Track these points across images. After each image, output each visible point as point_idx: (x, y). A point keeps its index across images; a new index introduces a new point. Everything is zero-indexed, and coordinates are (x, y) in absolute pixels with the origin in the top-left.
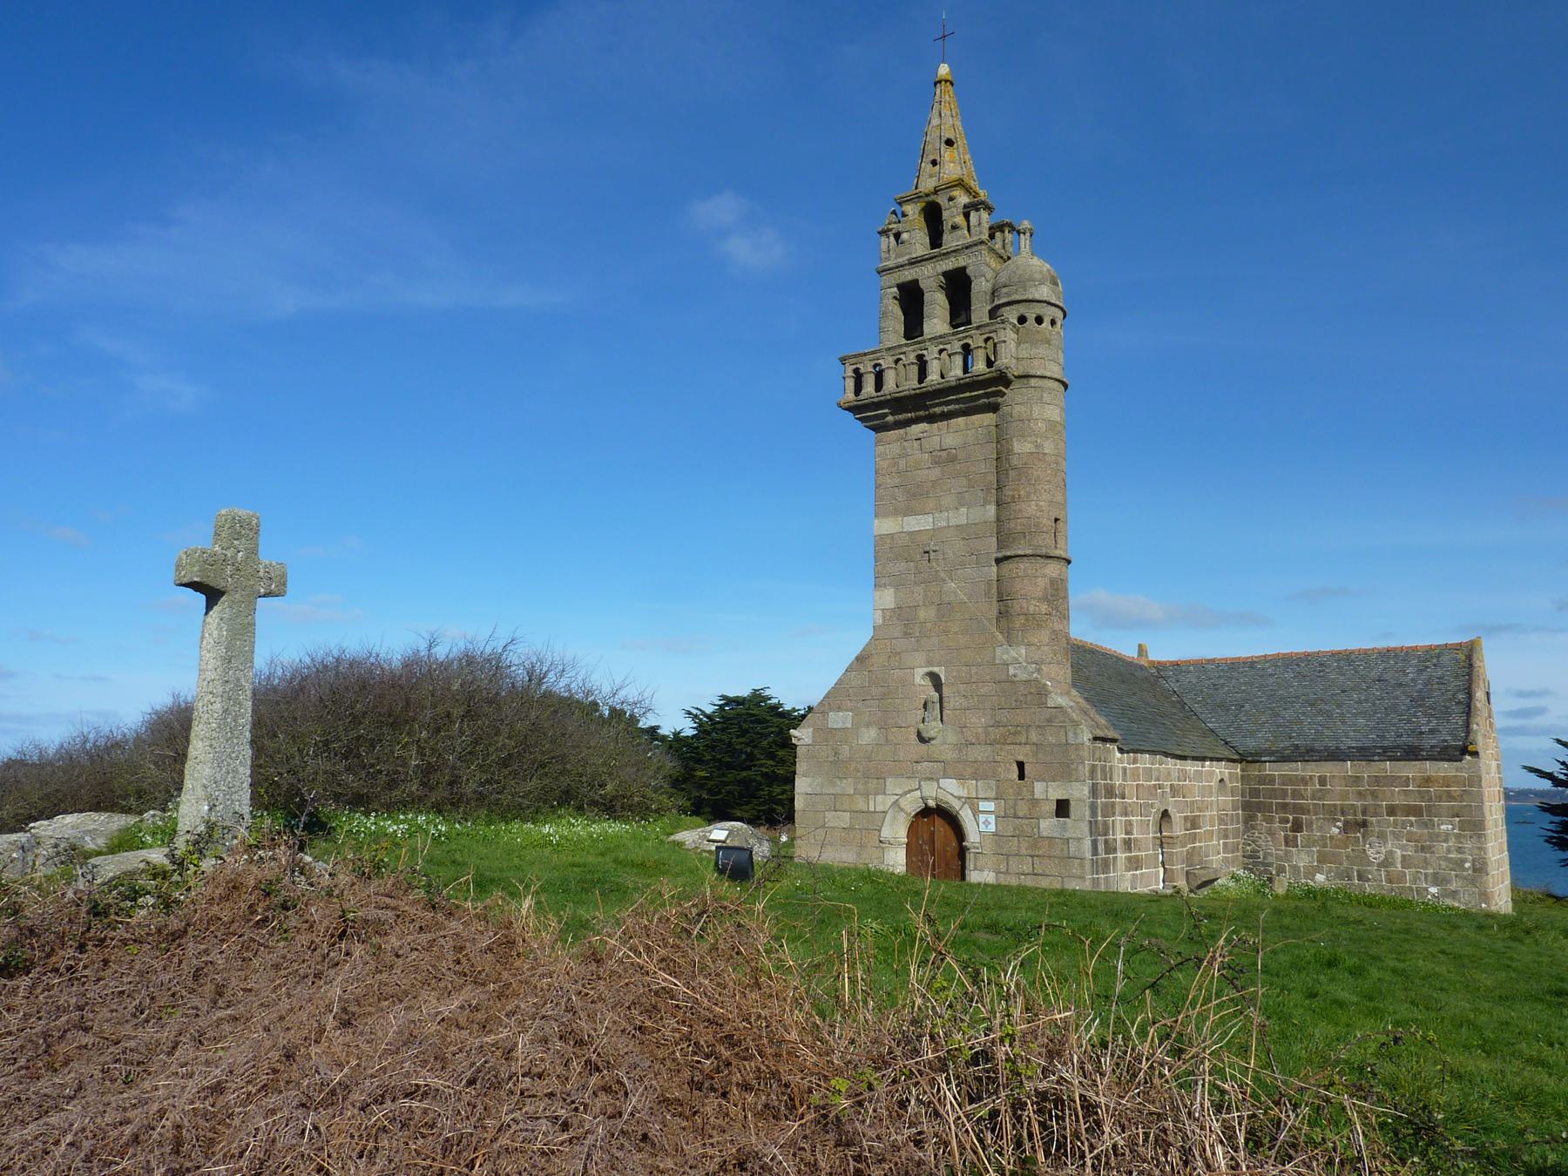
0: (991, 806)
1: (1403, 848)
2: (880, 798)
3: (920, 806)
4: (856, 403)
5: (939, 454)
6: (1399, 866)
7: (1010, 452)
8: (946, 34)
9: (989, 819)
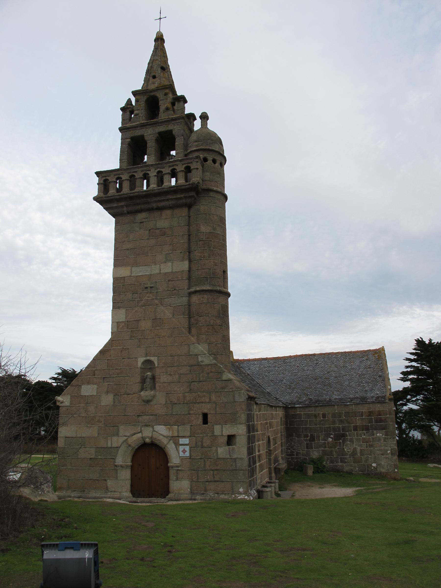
0: (186, 441)
1: (361, 446)
2: (115, 439)
3: (141, 442)
4: (104, 198)
6: (359, 455)
8: (161, 18)
9: (186, 449)
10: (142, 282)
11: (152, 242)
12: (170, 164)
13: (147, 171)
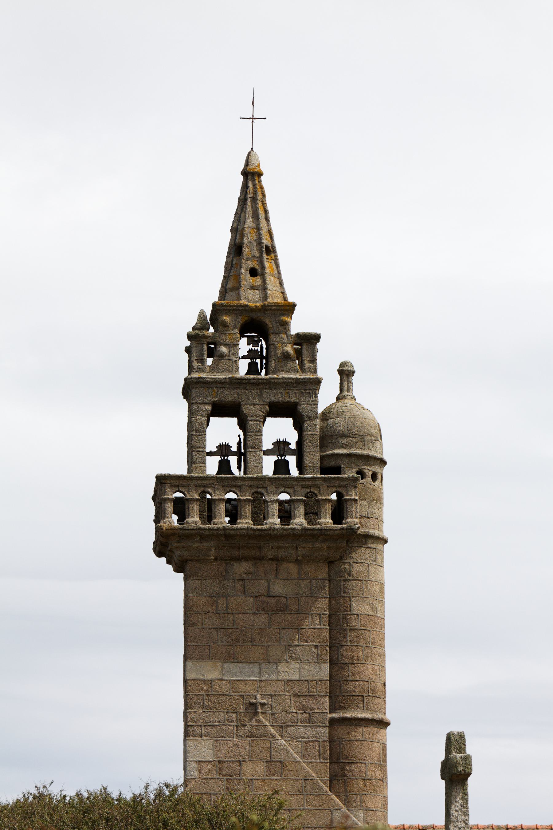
5: (266, 599)
7: (348, 611)
10: (245, 692)
11: (262, 620)
12: (304, 483)
13: (260, 488)
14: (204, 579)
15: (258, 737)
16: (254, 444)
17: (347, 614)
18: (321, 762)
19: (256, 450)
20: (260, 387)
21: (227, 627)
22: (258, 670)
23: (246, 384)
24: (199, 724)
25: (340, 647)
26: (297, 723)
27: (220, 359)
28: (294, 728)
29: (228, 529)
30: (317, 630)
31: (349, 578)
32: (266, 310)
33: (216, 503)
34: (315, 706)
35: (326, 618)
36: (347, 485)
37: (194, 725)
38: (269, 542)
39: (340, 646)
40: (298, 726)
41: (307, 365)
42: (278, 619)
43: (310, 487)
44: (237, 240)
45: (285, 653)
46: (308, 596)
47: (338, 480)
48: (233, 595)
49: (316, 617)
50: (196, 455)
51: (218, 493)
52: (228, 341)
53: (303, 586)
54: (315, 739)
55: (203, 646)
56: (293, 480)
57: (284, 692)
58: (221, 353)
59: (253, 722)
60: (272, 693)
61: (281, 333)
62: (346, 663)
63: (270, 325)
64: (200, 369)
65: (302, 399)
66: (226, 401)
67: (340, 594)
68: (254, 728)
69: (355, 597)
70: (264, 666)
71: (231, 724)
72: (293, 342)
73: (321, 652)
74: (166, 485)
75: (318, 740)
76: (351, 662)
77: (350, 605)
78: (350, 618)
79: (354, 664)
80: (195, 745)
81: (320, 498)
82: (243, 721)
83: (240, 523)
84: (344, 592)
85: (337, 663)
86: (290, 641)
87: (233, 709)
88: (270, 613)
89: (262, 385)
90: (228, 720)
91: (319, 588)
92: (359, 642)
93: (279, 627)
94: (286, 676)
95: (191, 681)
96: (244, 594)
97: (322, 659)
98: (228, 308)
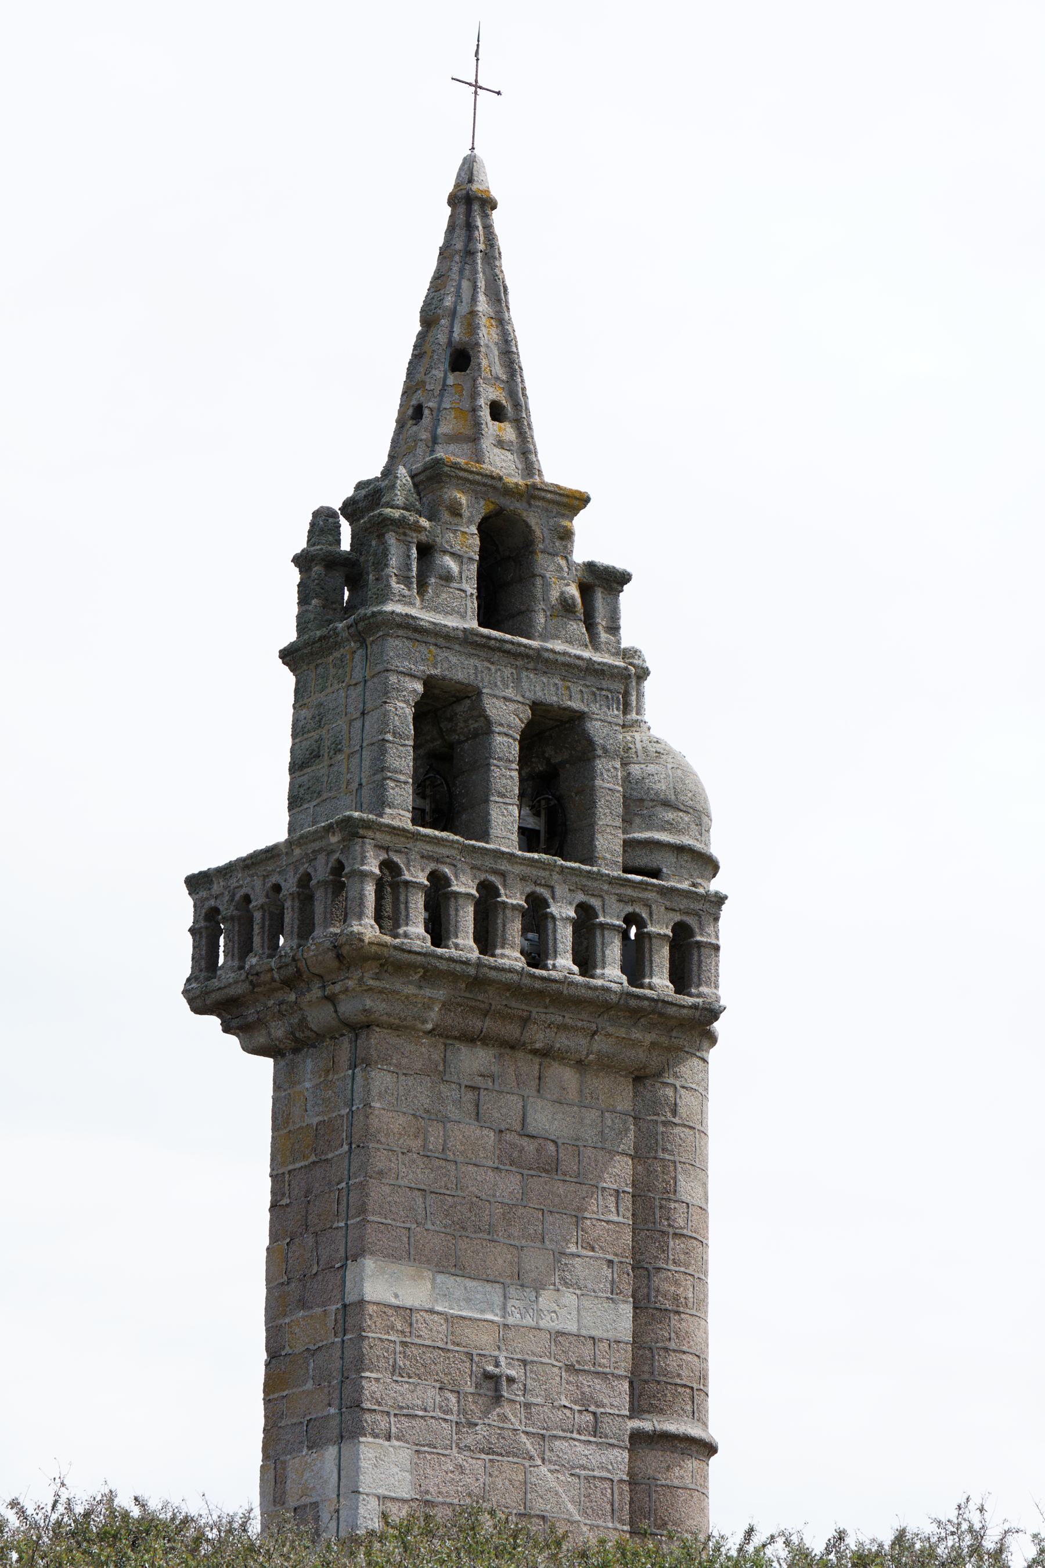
10: (476, 1347)
11: (509, 1185)
13: (540, 885)
14: (404, 1074)
15: (501, 1455)
16: (503, 787)
17: (670, 1200)
18: (615, 1529)
19: (508, 801)
20: (518, 663)
21: (442, 1191)
22: (502, 1299)
23: (493, 649)
24: (386, 1409)
25: (653, 1271)
26: (572, 1432)
27: (443, 583)
28: (567, 1444)
29: (485, 966)
30: (611, 1226)
31: (674, 1120)
32: (534, 497)
33: (460, 903)
34: (606, 1398)
35: (627, 1202)
36: (701, 912)
37: (375, 1410)
38: (547, 1011)
39: (654, 1268)
40: (574, 1439)
41: (604, 636)
42: (541, 1188)
43: (632, 902)
44: (455, 335)
45: (552, 1268)
46: (597, 1146)
47: (686, 897)
48: (457, 1118)
49: (611, 1195)
50: (393, 789)
51: (463, 879)
52: (459, 548)
53: (589, 1122)
54: (605, 1474)
55: (397, 1227)
56: (604, 881)
57: (550, 1358)
58: (449, 572)
59: (493, 1418)
60: (527, 1357)
61: (557, 556)
62: (666, 1310)
63: (538, 533)
64: (404, 596)
65: (594, 708)
66: (452, 680)
67: (656, 1151)
68: (495, 1433)
69: (684, 1163)
70: (512, 1291)
71: (447, 1417)
72: (579, 580)
73: (619, 1276)
74: (367, 841)
75: (610, 1476)
76: (675, 1308)
77: (675, 1178)
78: (675, 1208)
79: (678, 1313)
80: (376, 1457)
81: (653, 929)
82: (470, 1413)
83: (503, 956)
84: (663, 1150)
85: (646, 1308)
86: (562, 1243)
87: (451, 1382)
88: (526, 1172)
89: (523, 660)
90: (441, 1407)
91: (617, 1131)
92: (687, 1266)
93: (542, 1207)
94: (553, 1322)
95: (372, 1305)
96: (477, 1119)
97: (620, 1293)
98: (478, 478)
